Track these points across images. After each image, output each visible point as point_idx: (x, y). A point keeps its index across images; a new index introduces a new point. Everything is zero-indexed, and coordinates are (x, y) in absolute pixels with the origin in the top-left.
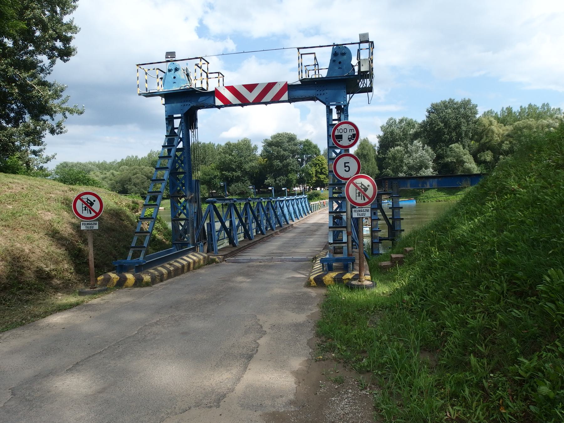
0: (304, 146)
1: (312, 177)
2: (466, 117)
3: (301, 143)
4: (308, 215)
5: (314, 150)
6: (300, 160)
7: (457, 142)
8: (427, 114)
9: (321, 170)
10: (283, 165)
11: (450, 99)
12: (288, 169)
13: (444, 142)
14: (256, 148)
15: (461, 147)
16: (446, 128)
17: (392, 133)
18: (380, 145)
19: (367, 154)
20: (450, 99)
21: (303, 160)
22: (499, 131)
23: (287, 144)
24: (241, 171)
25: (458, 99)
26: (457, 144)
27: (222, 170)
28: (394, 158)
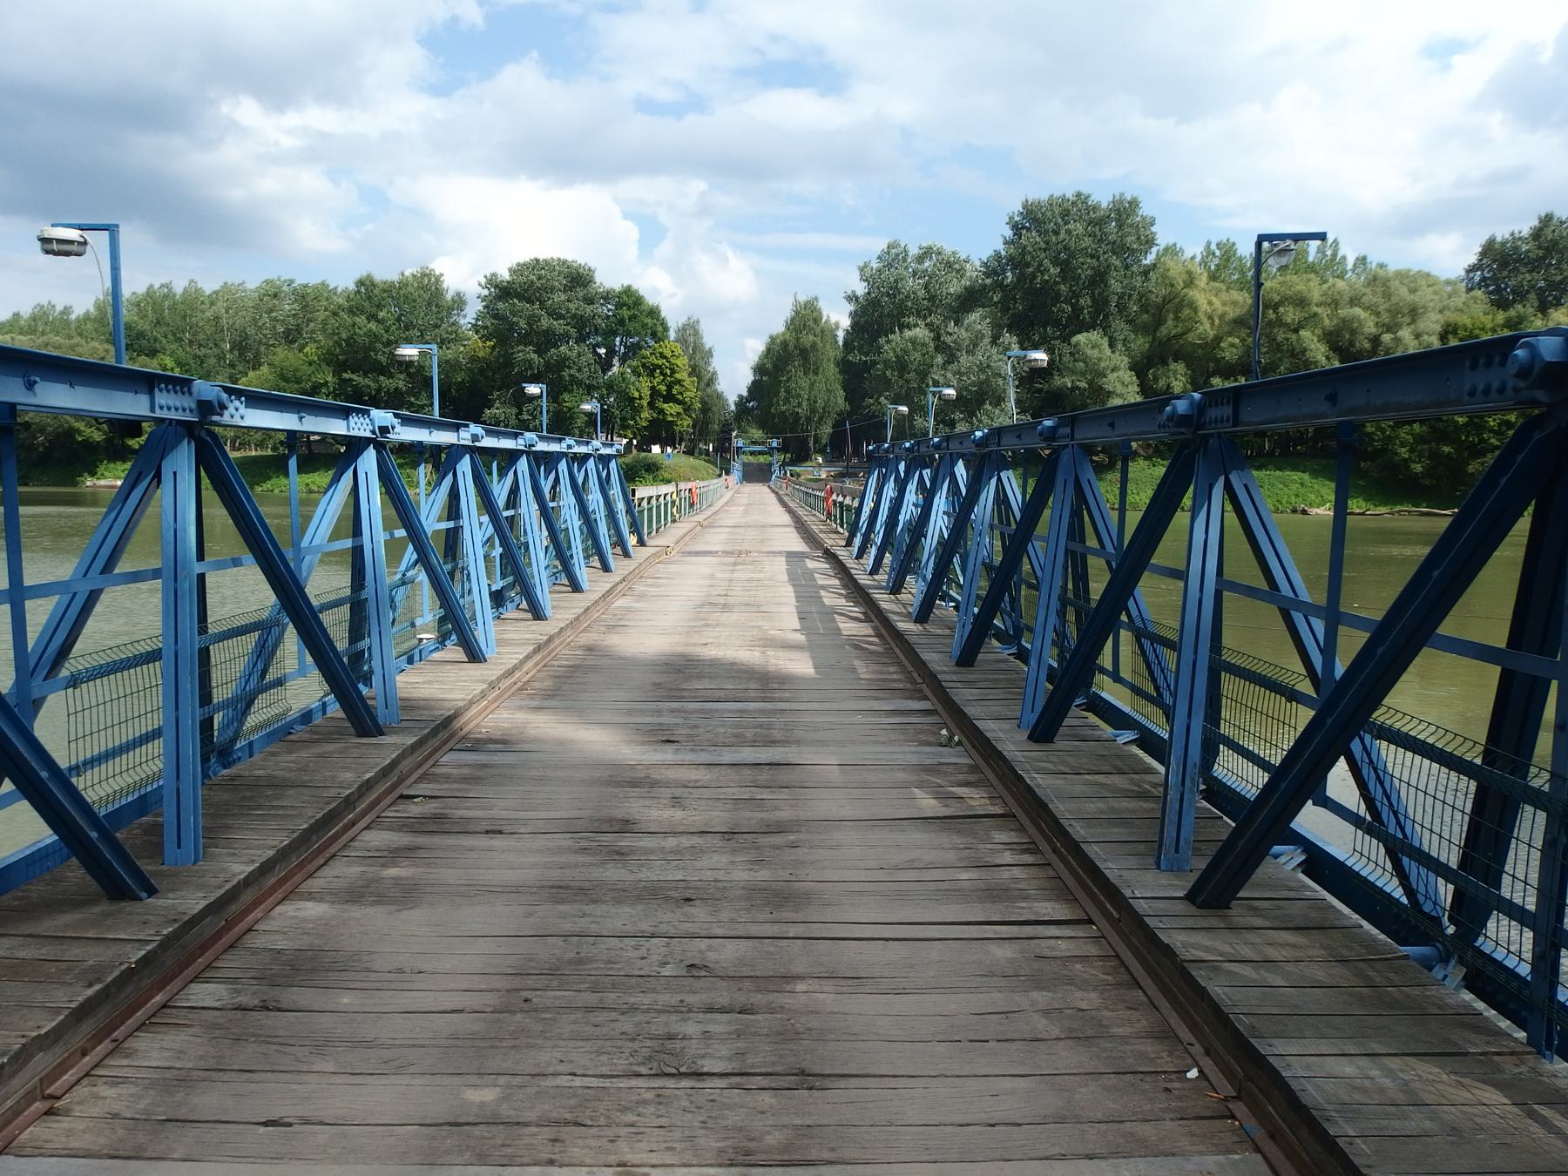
0: (619, 306)
1: (637, 410)
2: (1120, 249)
3: (607, 297)
4: (620, 566)
5: (649, 321)
6: (602, 351)
7: (1090, 327)
8: (1009, 233)
9: (670, 388)
10: (547, 364)
11: (1079, 195)
12: (561, 377)
13: (1057, 323)
14: (459, 302)
15: (1105, 343)
16: (1064, 280)
17: (895, 289)
18: (854, 325)
19: (814, 345)
20: (1079, 195)
21: (611, 352)
22: (1214, 305)
23: (563, 297)
24: (409, 375)
25: (1103, 198)
26: (1094, 336)
27: (339, 367)
28: (901, 365)
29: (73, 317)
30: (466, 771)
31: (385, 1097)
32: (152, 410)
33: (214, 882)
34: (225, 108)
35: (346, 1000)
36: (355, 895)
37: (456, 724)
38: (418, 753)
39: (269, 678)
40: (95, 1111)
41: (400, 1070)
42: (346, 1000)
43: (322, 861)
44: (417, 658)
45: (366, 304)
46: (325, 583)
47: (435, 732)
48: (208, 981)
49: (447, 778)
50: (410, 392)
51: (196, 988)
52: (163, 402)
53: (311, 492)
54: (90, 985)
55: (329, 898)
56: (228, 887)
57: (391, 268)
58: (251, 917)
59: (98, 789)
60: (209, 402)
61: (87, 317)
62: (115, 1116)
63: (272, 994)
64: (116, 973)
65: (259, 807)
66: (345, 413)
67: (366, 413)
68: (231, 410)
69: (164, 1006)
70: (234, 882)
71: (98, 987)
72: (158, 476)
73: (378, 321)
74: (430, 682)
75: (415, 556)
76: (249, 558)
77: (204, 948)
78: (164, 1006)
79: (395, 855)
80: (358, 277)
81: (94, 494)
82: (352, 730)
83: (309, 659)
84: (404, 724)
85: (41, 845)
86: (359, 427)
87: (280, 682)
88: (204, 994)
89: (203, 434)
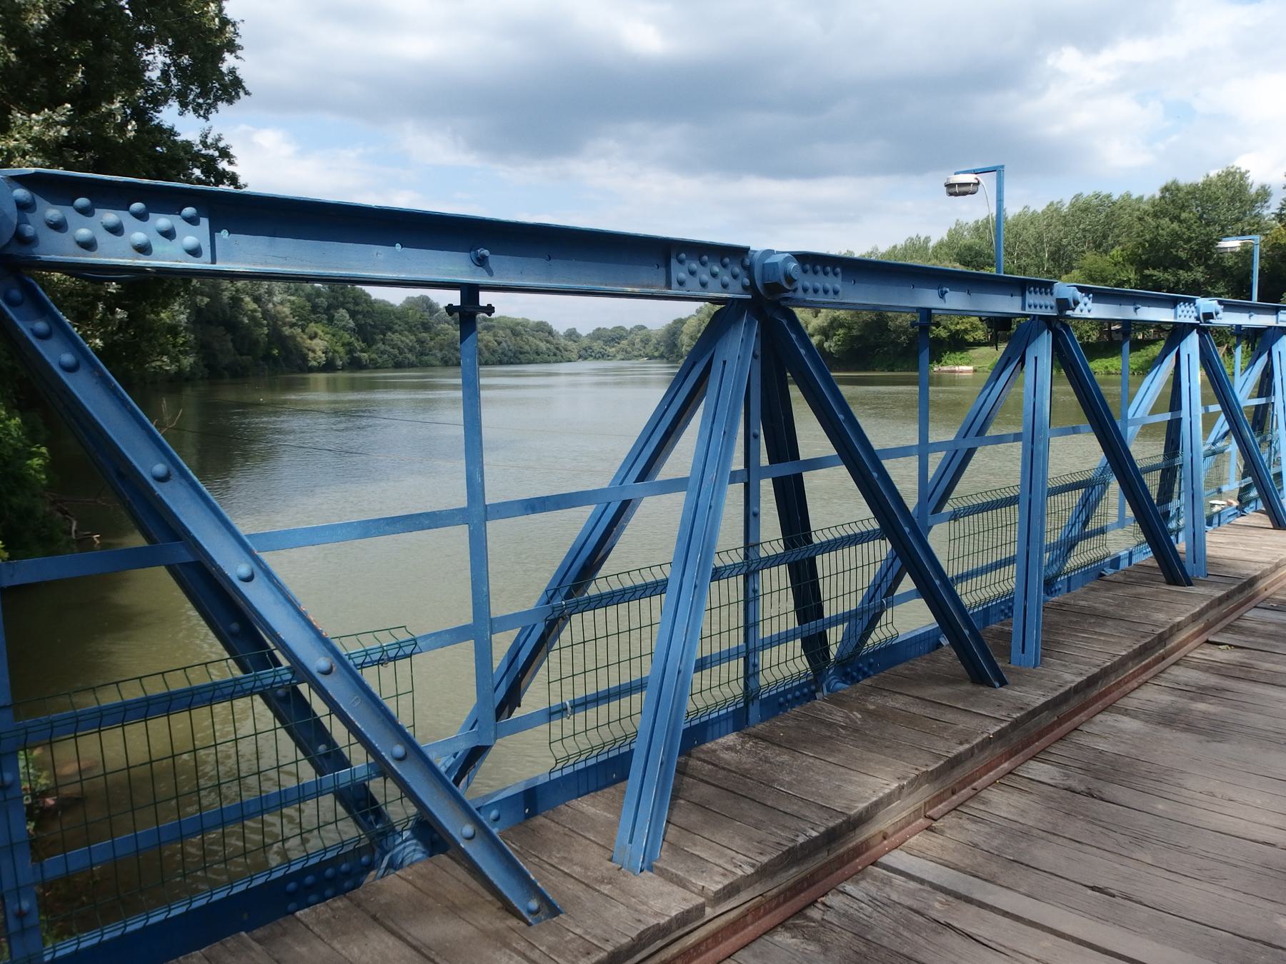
24: (1208, 267)
27: (1141, 265)
29: (931, 244)
30: (1271, 628)
31: (1196, 897)
32: (1023, 308)
33: (1050, 685)
34: (1050, 62)
35: (1161, 806)
36: (1168, 719)
37: (1261, 585)
38: (1224, 606)
39: (1092, 526)
40: (961, 837)
41: (1213, 880)
42: (1160, 807)
43: (1136, 685)
44: (1216, 520)
45: (1170, 208)
46: (1145, 452)
47: (1242, 589)
48: (1044, 761)
49: (1252, 632)
50: (1207, 282)
51: (1033, 764)
52: (1032, 302)
53: (1109, 373)
54: (961, 744)
55: (1142, 716)
56: (1062, 690)
57: (1194, 172)
58: (1076, 719)
59: (972, 595)
60: (1066, 300)
61: (941, 245)
62: (976, 846)
63: (1095, 785)
64: (979, 739)
65: (1084, 631)
66: (1173, 303)
67: (1192, 301)
68: (1081, 305)
69: (1010, 773)
70: (1067, 688)
71: (967, 746)
72: (1022, 361)
73: (1181, 221)
74: (1234, 544)
75: (1227, 427)
76: (1086, 425)
77: (1040, 735)
78: (1010, 773)
79: (1202, 692)
80: (1163, 184)
81: (939, 377)
82: (1163, 579)
83: (1129, 512)
84: (1210, 578)
85: (917, 633)
86: (1185, 314)
87: (1102, 531)
88: (1038, 770)
89: (1058, 326)
